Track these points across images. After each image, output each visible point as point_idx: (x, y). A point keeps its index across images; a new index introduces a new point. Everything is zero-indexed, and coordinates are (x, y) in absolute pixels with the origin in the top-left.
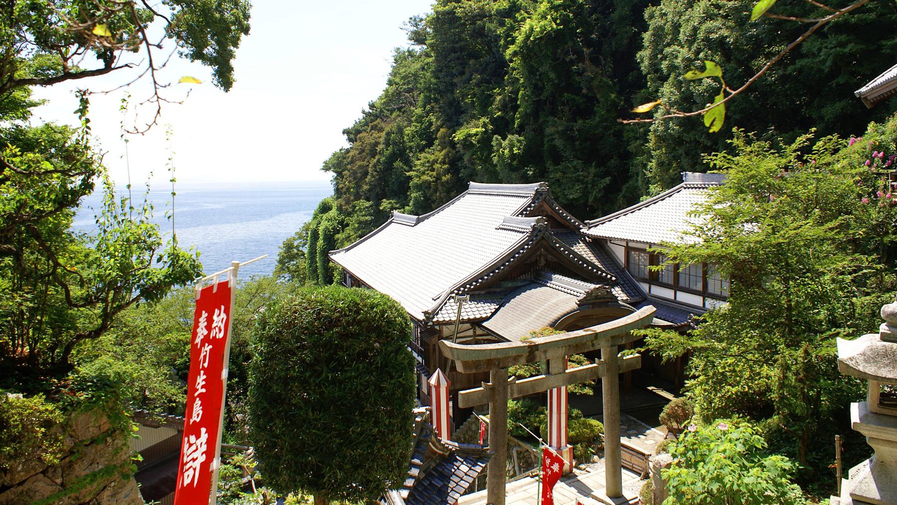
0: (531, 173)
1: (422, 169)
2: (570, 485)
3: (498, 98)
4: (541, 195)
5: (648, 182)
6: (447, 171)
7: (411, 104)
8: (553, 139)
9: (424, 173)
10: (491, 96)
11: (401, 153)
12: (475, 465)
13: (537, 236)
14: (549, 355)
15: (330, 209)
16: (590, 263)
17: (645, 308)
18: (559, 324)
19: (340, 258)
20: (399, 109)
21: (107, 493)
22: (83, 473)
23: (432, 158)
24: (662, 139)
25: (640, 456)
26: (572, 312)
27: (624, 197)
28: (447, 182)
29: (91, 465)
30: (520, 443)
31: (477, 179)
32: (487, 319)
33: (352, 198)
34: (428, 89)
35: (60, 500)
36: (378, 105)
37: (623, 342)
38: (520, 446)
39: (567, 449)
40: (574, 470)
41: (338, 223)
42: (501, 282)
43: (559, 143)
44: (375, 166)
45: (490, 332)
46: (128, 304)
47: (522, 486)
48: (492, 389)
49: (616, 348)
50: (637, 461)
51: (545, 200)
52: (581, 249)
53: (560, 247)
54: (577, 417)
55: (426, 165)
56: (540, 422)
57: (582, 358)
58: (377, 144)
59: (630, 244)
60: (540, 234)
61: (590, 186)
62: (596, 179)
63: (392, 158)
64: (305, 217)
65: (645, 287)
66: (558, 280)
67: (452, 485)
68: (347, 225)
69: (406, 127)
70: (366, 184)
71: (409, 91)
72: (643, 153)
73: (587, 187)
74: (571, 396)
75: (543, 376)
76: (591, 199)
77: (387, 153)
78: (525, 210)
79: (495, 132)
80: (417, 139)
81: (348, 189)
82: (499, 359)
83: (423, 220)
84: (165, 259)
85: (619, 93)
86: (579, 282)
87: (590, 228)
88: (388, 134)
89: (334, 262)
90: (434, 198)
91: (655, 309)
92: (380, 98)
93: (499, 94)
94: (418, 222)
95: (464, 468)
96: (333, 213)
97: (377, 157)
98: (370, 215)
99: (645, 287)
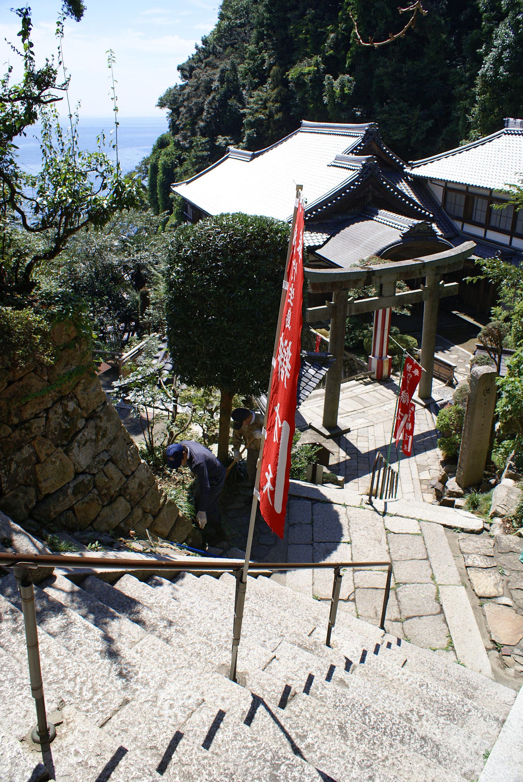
0: (359, 113)
1: (255, 107)
2: (388, 388)
3: (332, 35)
4: (371, 135)
5: (468, 127)
6: (278, 111)
7: (244, 41)
8: (382, 80)
9: (257, 111)
10: (324, 33)
11: (233, 90)
12: (320, 369)
13: (367, 173)
14: (383, 280)
15: (168, 144)
16: (411, 200)
17: (466, 243)
18: (386, 254)
19: (184, 190)
20: (232, 45)
21: (80, 388)
22: (62, 372)
23: (264, 95)
24: (490, 84)
25: (447, 367)
26: (396, 243)
27: (443, 140)
28: (279, 120)
29: (66, 365)
30: (346, 353)
31: (315, 119)
32: (320, 247)
33: (189, 134)
34: (261, 24)
35: (50, 393)
36: (211, 39)
37: (446, 272)
38: (345, 355)
39: (387, 359)
40: (391, 376)
41: (176, 158)
42: (334, 214)
43: (387, 84)
44: (210, 103)
45: (322, 259)
46: (79, 228)
47: (348, 388)
48: (334, 307)
49: (439, 277)
50: (443, 371)
51: (374, 139)
52: (403, 187)
53: (386, 185)
54: (395, 334)
55: (256, 102)
56: (364, 336)
57: (403, 284)
58: (212, 81)
59: (449, 185)
60: (370, 172)
61: (413, 128)
62: (420, 121)
63: (226, 97)
64: (146, 151)
65: (458, 224)
66: (383, 214)
67: (303, 384)
68: (185, 160)
69: (239, 64)
70: (202, 121)
71: (242, 25)
72: (467, 97)
73: (410, 129)
74: (393, 315)
75: (377, 298)
76: (413, 140)
77: (222, 91)
78: (356, 148)
79: (326, 72)
80: (249, 77)
81: (185, 125)
82: (342, 282)
83: (257, 155)
84: (109, 186)
85: (450, 34)
86: (403, 217)
87: (413, 168)
88: (223, 71)
89: (174, 192)
90: (266, 135)
91: (475, 245)
92: (213, 33)
93: (332, 32)
94: (254, 157)
95: (312, 371)
96: (171, 148)
97: (212, 95)
98: (206, 150)
99: (458, 224)
